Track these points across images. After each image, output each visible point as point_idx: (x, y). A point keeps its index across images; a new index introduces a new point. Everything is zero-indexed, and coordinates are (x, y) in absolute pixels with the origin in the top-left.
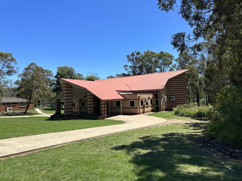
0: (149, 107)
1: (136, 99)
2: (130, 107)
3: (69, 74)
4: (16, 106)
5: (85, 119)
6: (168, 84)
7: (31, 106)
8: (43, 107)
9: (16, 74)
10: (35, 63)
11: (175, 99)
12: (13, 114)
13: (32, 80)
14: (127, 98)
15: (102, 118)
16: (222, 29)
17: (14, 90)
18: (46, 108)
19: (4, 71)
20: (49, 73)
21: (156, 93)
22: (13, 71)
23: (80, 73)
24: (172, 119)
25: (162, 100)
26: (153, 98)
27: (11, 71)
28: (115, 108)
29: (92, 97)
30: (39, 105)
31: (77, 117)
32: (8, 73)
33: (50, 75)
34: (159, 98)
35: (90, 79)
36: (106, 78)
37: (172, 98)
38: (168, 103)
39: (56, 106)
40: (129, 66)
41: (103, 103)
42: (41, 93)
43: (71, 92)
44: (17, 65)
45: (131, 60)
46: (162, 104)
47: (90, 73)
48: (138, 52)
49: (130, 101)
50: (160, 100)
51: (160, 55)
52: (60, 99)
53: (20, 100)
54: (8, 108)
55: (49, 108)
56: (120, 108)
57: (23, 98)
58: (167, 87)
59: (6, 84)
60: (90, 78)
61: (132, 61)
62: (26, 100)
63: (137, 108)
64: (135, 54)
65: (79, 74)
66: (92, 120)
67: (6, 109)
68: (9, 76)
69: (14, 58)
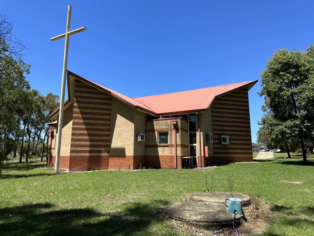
6: (214, 106)
37: (225, 140)
43: (108, 117)
49: (144, 135)
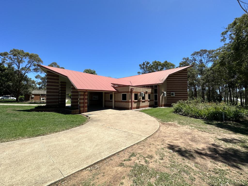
0: (146, 102)
1: (128, 92)
2: (122, 100)
11: (175, 96)
14: (119, 91)
15: (79, 112)
16: (208, 52)
21: (155, 88)
24: (170, 123)
25: (162, 95)
26: (151, 93)
28: (122, 102)
31: (54, 109)
34: (158, 92)
37: (173, 94)
38: (168, 99)
40: (141, 73)
41: (83, 93)
45: (142, 68)
46: (161, 101)
48: (148, 62)
50: (159, 95)
54: (41, 98)
56: (112, 101)
58: (167, 81)
61: (143, 69)
63: (129, 102)
64: (145, 64)
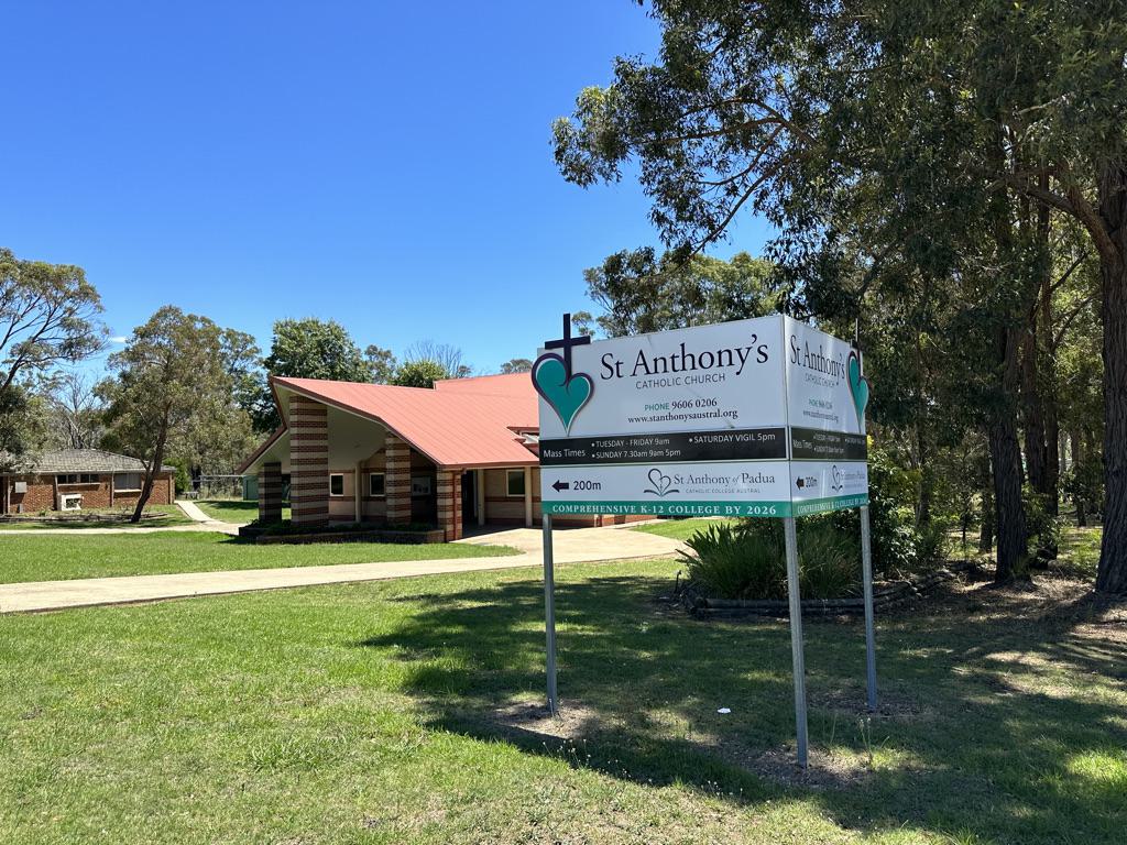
3: (323, 352)
4: (96, 488)
5: (372, 541)
7: (160, 487)
8: (214, 493)
9: (99, 355)
10: (177, 310)
12: (87, 522)
13: (165, 381)
17: (90, 420)
18: (227, 500)
19: (50, 342)
20: (241, 343)
22: (88, 340)
23: (383, 347)
27: (80, 342)
29: (408, 452)
30: (196, 486)
32: (65, 349)
33: (248, 356)
35: (417, 379)
36: (498, 369)
39: (262, 491)
40: (594, 317)
42: (204, 433)
43: (320, 430)
44: (104, 317)
47: (427, 346)
51: (734, 271)
52: (281, 460)
53: (115, 463)
54: (64, 498)
55: (239, 499)
56: (523, 500)
57: (127, 454)
59: (53, 393)
60: (416, 372)
62: (140, 464)
65: (375, 349)
66: (404, 543)
67: (55, 499)
68: (70, 363)
69: (91, 289)
